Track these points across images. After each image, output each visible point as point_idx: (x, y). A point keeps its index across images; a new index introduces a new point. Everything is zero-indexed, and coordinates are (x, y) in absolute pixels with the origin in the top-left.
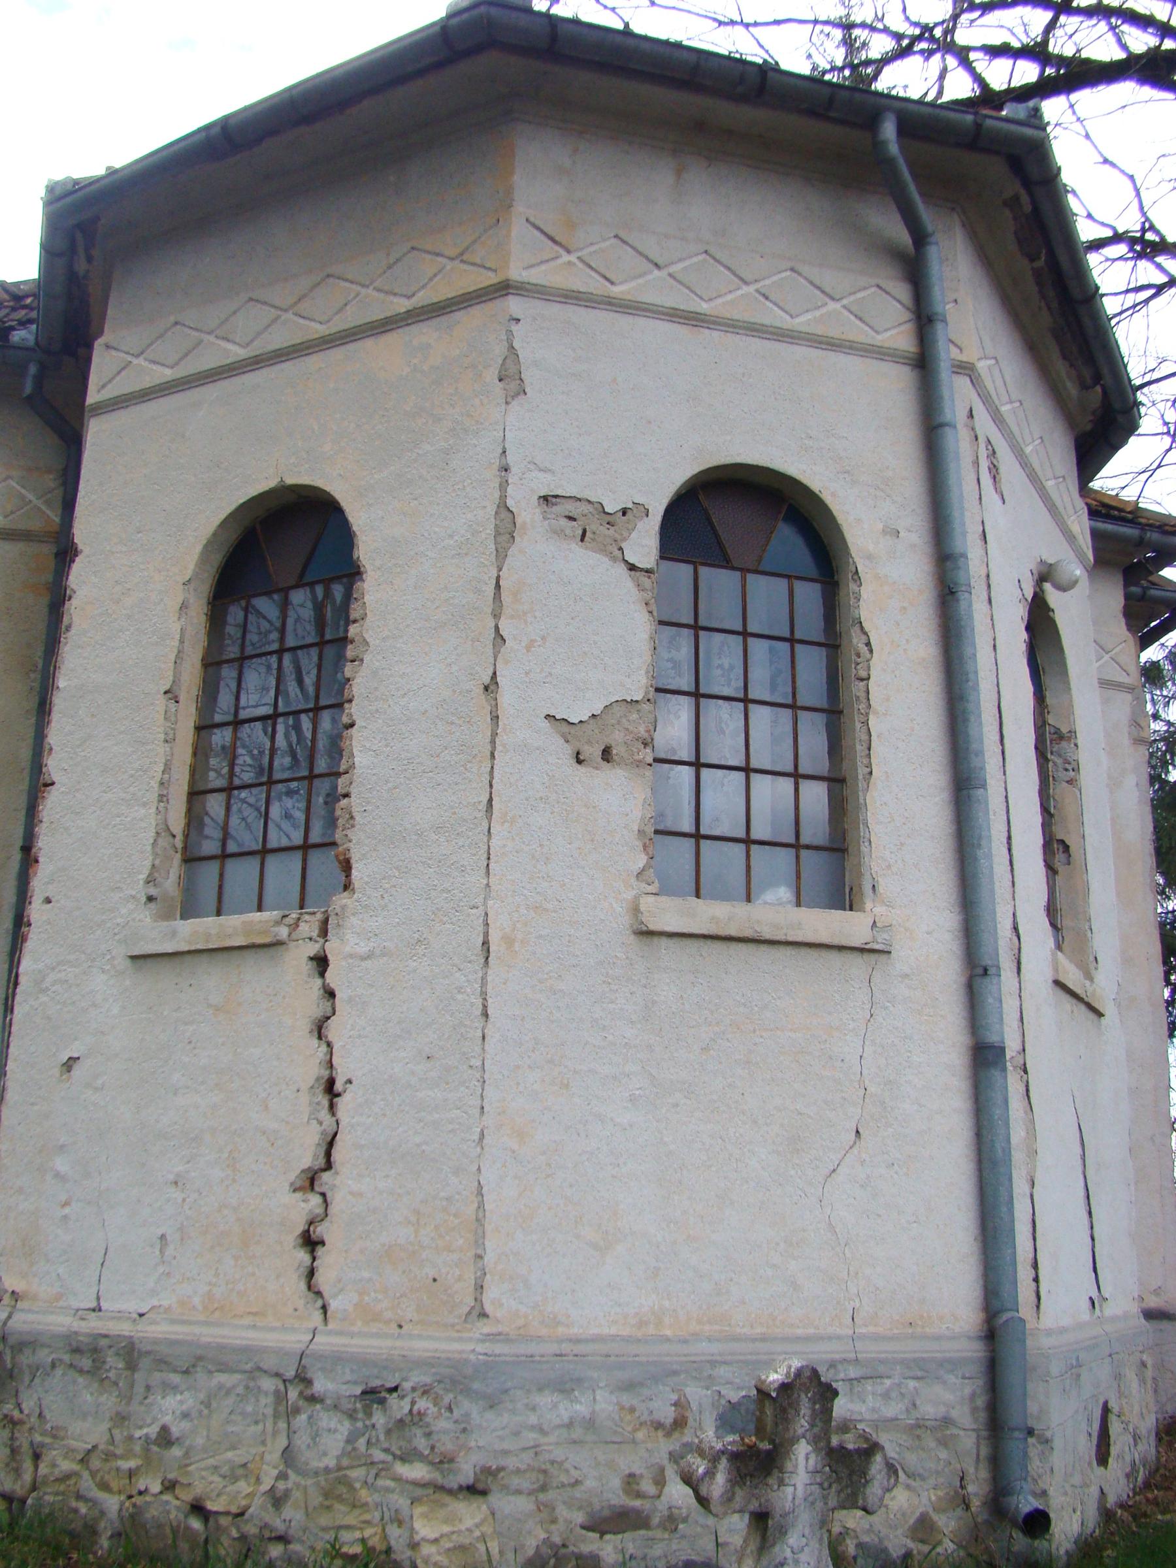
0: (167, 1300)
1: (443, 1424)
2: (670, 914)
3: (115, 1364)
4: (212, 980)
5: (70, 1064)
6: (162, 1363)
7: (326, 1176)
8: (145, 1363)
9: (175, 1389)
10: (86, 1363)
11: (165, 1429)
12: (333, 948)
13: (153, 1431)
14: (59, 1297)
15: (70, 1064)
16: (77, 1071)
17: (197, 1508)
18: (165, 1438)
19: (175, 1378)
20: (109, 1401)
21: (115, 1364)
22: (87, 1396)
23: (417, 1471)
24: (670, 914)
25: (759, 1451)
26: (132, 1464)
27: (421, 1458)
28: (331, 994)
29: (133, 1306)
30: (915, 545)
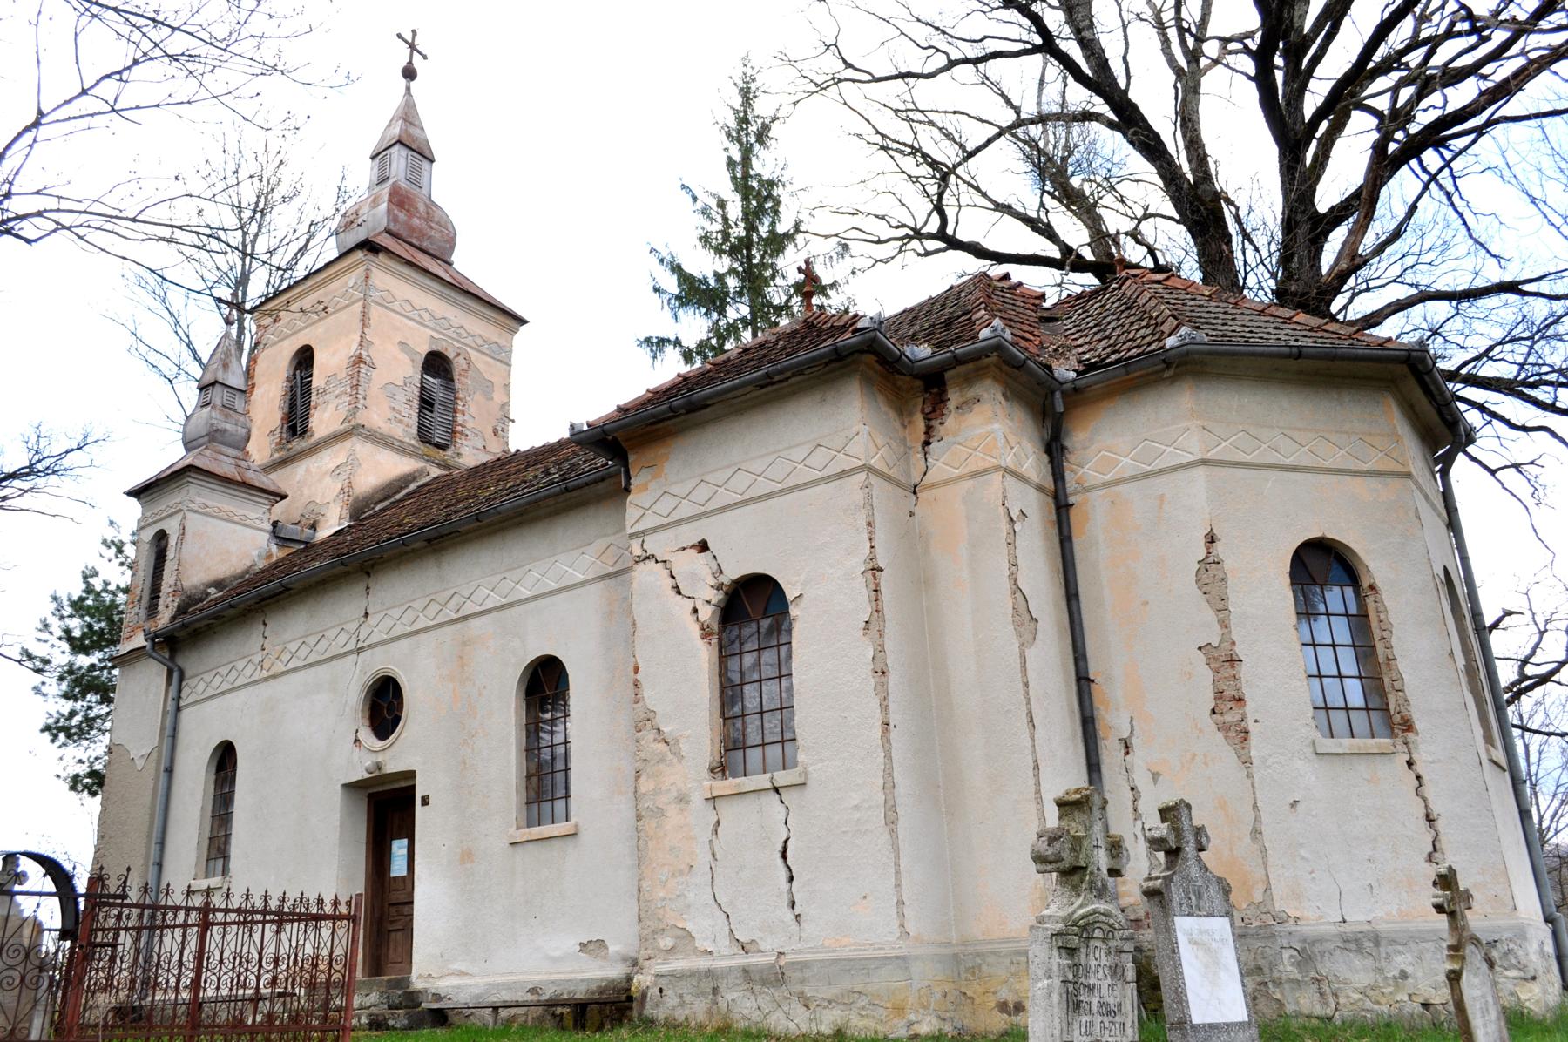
0: (1380, 914)
1: (1520, 953)
2: (1328, 745)
3: (1368, 945)
4: (1362, 766)
5: (1294, 804)
6: (1393, 942)
7: (1436, 855)
8: (1383, 943)
9: (1401, 953)
10: (1353, 947)
11: (1402, 971)
12: (1415, 757)
13: (1396, 973)
14: (1320, 917)
15: (1294, 804)
16: (1299, 807)
17: (1426, 1005)
18: (1404, 975)
19: (1400, 948)
20: (1369, 962)
21: (1368, 945)
22: (1357, 961)
23: (1514, 973)
24: (1328, 745)
25: (35, 945)
26: (1391, 989)
27: (1515, 967)
28: (1418, 777)
29: (1363, 918)
30: (314, 527)
